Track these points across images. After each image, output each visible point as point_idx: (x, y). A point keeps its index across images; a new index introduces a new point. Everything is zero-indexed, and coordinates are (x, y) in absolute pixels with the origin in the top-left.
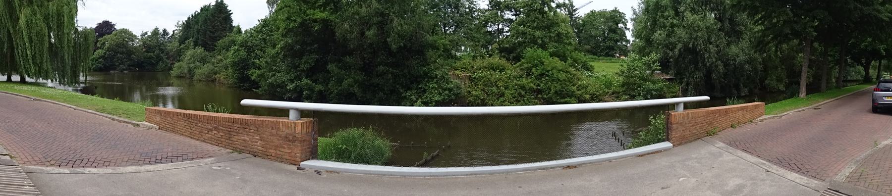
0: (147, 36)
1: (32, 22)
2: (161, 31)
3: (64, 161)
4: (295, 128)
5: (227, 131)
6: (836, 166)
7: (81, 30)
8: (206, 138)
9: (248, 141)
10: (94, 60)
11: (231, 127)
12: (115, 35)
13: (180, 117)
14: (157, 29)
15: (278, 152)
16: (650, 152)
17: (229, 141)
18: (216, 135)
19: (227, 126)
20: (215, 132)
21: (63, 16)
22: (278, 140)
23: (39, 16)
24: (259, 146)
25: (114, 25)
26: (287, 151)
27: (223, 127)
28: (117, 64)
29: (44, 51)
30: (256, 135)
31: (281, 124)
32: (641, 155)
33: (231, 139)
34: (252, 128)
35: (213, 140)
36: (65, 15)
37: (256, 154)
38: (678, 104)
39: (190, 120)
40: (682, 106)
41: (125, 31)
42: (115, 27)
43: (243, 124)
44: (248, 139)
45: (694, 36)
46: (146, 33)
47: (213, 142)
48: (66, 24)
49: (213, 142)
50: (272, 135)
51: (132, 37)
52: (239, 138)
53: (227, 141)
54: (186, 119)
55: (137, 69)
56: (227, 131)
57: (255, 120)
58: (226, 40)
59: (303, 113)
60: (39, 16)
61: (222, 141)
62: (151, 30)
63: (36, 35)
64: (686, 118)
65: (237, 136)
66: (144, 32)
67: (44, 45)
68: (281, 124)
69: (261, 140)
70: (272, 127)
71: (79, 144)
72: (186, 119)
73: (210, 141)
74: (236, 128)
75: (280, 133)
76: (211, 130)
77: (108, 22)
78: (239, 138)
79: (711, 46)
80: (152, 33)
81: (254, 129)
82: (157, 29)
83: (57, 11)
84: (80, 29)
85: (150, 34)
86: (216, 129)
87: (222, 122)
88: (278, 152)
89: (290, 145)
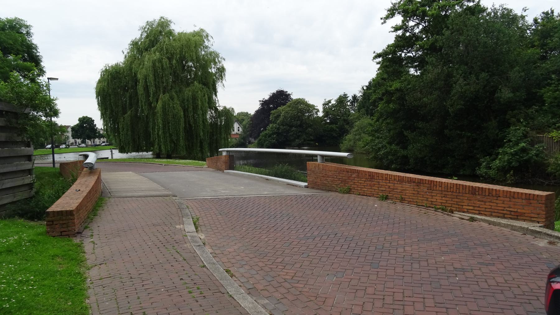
0: (330, 104)
1: (169, 106)
2: (350, 98)
3: (271, 258)
7: (222, 108)
10: (267, 136)
12: (289, 107)
14: (345, 95)
16: (290, 184)
21: (198, 100)
23: (176, 100)
25: (289, 94)
28: (292, 138)
29: (180, 130)
32: (288, 184)
36: (199, 100)
41: (301, 102)
42: (292, 97)
46: (330, 102)
48: (200, 107)
51: (310, 108)
55: (317, 144)
58: (112, 132)
60: (176, 100)
62: (336, 97)
63: (173, 117)
64: (317, 168)
66: (327, 100)
67: (181, 125)
71: (279, 235)
77: (283, 91)
80: (336, 101)
82: (345, 95)
83: (192, 96)
84: (220, 109)
85: (335, 102)
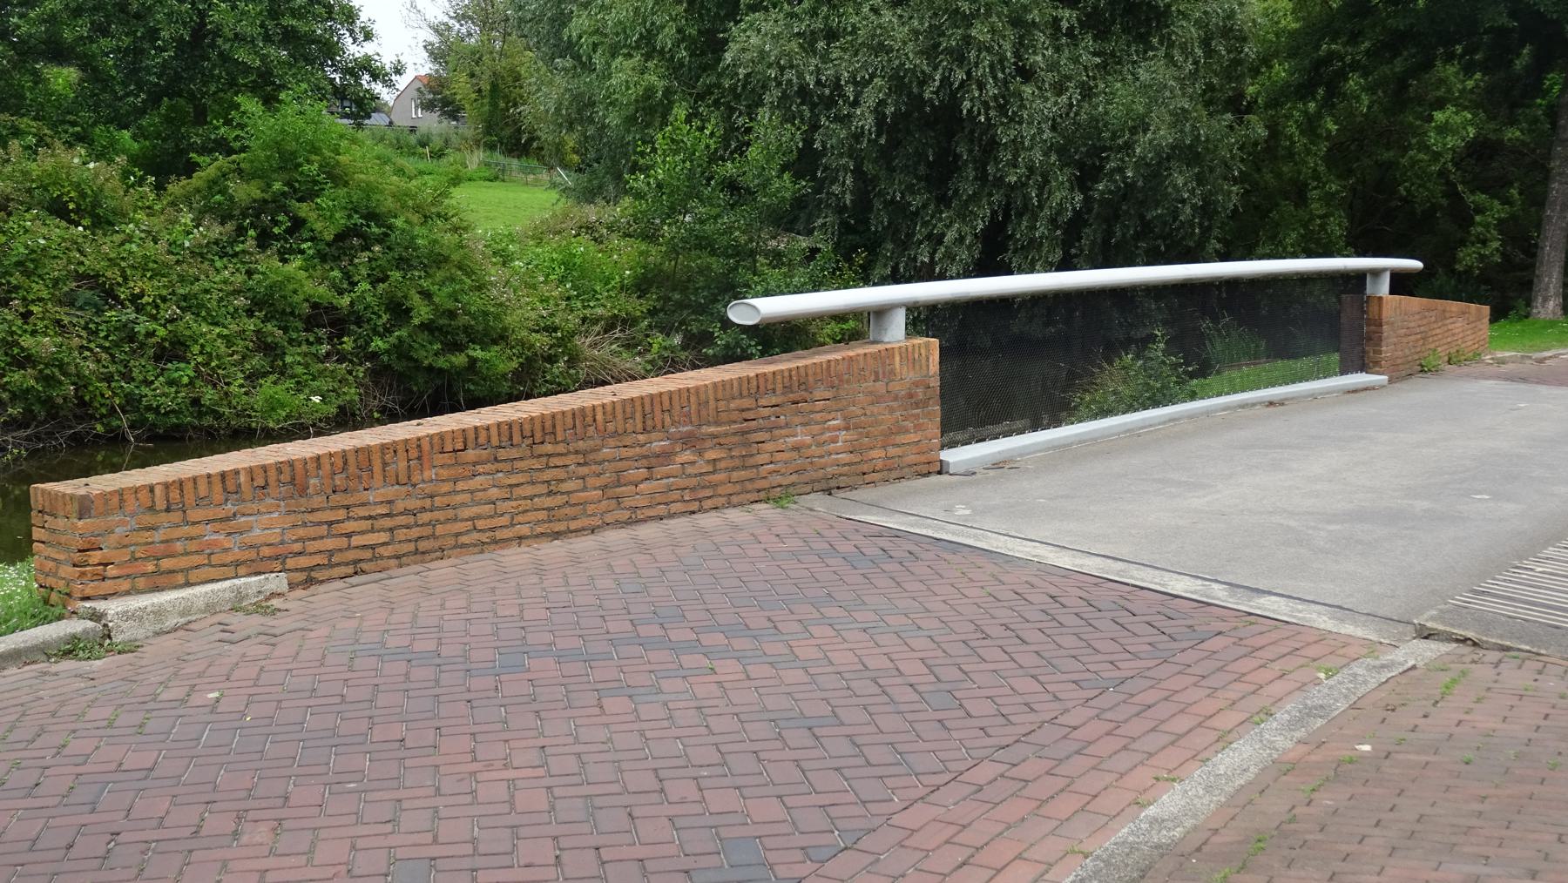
4: (928, 358)
5: (735, 434)
6: (1123, 762)
8: (640, 501)
9: (809, 446)
11: (750, 415)
13: (471, 454)
15: (892, 451)
17: (743, 474)
18: (690, 470)
19: (735, 416)
20: (687, 456)
22: (892, 410)
24: (838, 449)
26: (913, 437)
27: (717, 423)
30: (833, 415)
31: (897, 358)
33: (751, 461)
34: (818, 394)
35: (676, 495)
37: (833, 483)
38: (880, 313)
39: (548, 448)
40: (899, 321)
43: (790, 387)
44: (808, 439)
45: (952, 40)
47: (675, 507)
49: (675, 507)
50: (877, 399)
52: (780, 444)
53: (735, 475)
54: (514, 453)
56: (735, 434)
57: (790, 370)
59: (923, 318)
61: (714, 486)
65: (773, 439)
68: (897, 358)
69: (847, 429)
70: (877, 373)
72: (514, 453)
73: (662, 509)
74: (766, 412)
75: (896, 387)
76: (666, 456)
78: (780, 444)
79: (1028, 90)
81: (827, 394)
86: (689, 441)
87: (712, 403)
88: (892, 451)
89: (917, 417)
